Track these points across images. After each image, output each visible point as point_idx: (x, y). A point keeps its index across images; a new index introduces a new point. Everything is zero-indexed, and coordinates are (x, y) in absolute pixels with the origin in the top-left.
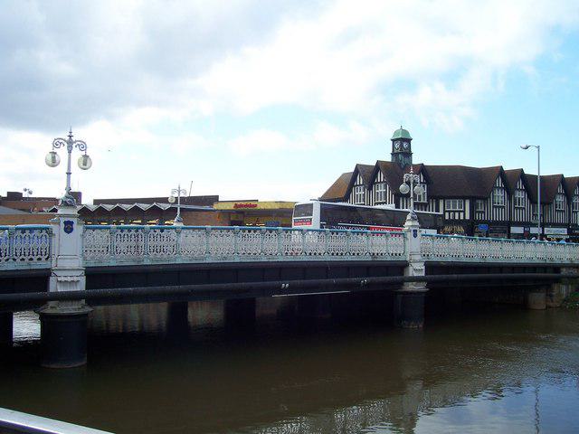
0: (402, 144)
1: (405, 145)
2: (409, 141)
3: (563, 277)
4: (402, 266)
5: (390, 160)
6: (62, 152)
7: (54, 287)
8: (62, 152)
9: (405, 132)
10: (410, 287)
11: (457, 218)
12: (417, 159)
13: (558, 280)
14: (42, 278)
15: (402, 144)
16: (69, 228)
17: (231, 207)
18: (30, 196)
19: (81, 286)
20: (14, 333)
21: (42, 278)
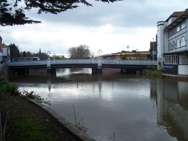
4: (97, 64)
8: (99, 51)
10: (98, 68)
13: (146, 68)
19: (50, 66)
20: (149, 90)
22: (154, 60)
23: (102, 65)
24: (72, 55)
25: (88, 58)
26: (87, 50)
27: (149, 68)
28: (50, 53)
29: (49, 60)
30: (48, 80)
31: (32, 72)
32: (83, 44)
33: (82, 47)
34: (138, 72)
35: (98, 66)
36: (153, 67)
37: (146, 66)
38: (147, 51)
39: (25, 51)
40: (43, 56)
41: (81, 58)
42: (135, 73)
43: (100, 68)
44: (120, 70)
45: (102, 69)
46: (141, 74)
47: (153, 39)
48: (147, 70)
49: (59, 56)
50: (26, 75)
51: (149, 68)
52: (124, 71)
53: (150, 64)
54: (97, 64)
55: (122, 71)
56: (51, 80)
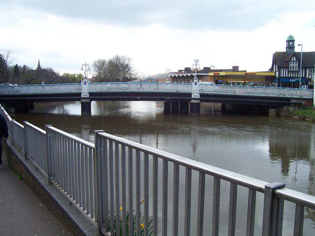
0: (291, 42)
1: (291, 43)
2: (293, 41)
3: (292, 103)
4: (190, 94)
5: (285, 50)
6: (84, 67)
7: (82, 96)
8: (84, 67)
9: (292, 37)
10: (193, 101)
11: (289, 76)
12: (297, 49)
13: (289, 105)
14: (80, 94)
15: (291, 42)
16: (85, 84)
17: (243, 74)
18: (214, 69)
19: (88, 96)
20: (81, 106)
21: (80, 94)
22: (231, 85)
23: (201, 95)
24: (100, 73)
25: (130, 80)
26: (127, 65)
27: (295, 105)
28: (87, 67)
29: (85, 84)
30: (83, 126)
31: (38, 106)
32: (120, 55)
33: (118, 59)
34: (272, 112)
35: (193, 97)
36: (304, 102)
37: (289, 99)
38: (230, 69)
39: (18, 66)
40: (44, 75)
41: (118, 80)
42: (267, 114)
43: (196, 101)
44: (221, 104)
45: (199, 104)
46: (278, 115)
47: (300, 45)
48: (291, 109)
49: (74, 75)
50: (30, 111)
51: (295, 105)
52: (228, 106)
53: (296, 97)
54: (190, 94)
55: (223, 107)
56: (88, 126)
